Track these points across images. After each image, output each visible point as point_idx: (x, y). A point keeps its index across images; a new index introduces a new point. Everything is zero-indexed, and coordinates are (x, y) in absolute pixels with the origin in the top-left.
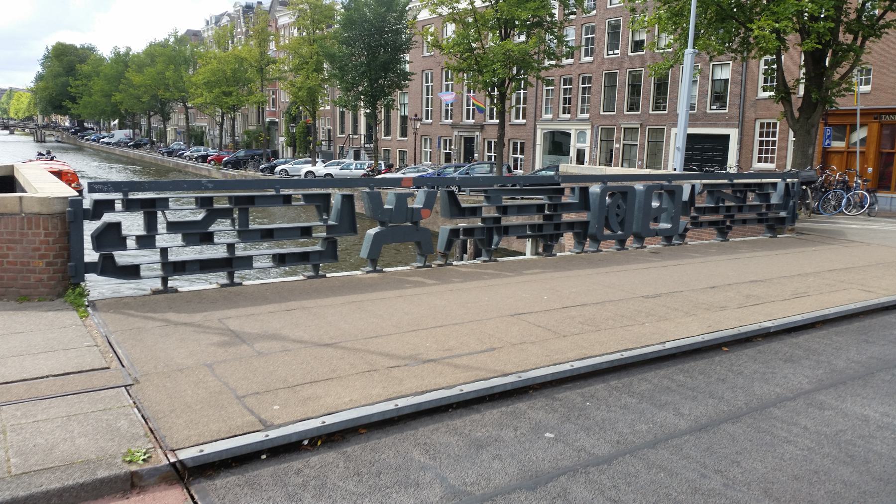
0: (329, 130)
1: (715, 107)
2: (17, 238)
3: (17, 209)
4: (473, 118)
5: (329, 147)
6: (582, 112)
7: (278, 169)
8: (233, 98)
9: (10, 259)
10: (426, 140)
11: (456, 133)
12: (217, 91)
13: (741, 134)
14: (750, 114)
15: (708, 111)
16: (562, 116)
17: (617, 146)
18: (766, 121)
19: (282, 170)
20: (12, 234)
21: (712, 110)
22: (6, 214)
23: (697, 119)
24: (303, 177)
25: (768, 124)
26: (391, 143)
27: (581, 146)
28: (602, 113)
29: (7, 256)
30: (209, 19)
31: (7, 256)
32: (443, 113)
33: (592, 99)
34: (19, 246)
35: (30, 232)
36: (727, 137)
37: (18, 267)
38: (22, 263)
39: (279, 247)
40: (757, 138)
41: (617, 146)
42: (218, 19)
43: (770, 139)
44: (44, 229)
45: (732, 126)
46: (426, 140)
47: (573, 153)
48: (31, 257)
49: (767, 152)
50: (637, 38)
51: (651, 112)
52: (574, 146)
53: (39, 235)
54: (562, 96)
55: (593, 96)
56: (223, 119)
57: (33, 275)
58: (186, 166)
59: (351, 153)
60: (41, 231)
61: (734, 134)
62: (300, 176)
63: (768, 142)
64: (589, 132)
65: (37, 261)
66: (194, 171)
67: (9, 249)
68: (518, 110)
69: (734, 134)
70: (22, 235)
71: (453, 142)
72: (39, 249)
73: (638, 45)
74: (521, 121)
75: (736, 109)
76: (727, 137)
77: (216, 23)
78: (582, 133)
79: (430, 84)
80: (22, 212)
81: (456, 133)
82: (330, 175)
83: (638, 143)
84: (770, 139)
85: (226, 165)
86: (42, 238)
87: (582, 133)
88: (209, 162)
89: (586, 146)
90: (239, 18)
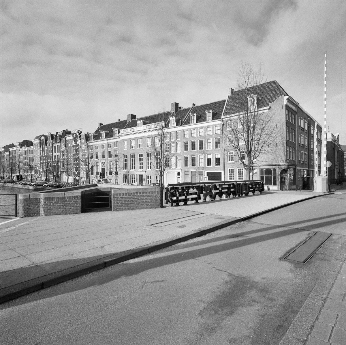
16: (229, 162)
32: (131, 168)
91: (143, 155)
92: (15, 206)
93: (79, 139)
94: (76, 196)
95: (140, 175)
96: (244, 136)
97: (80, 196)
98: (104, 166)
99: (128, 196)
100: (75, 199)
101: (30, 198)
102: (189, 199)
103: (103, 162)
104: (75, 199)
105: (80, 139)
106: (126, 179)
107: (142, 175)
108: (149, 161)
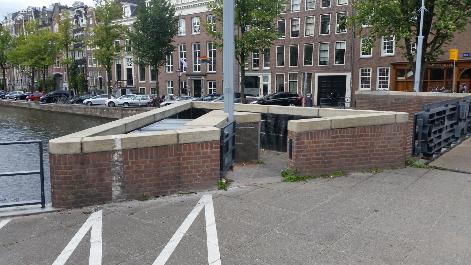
0: (100, 79)
1: (337, 63)
2: (392, 136)
3: (393, 122)
4: (199, 70)
5: (101, 87)
6: (265, 66)
7: (85, 101)
8: (46, 61)
9: (388, 148)
10: (169, 82)
11: (189, 78)
12: (36, 58)
13: (352, 75)
14: (357, 65)
15: (334, 65)
16: (254, 68)
17: (286, 83)
18: (382, 68)
19: (88, 102)
20: (390, 134)
21: (336, 64)
22: (389, 124)
23: (329, 69)
24: (107, 105)
25: (366, 70)
26: (146, 85)
27: (265, 83)
28: (276, 67)
29: (387, 146)
30: (6, 16)
31: (387, 146)
32: (208, 68)
33: (271, 60)
34: (392, 141)
35: (398, 133)
36: (345, 77)
37: (391, 151)
38: (393, 150)
39: (68, 145)
40: (360, 77)
41: (286, 83)
42: (15, 15)
43: (367, 77)
44: (404, 131)
45: (348, 72)
46: (169, 82)
47: (261, 87)
48: (397, 146)
49: (383, 82)
50: (294, 30)
51: (304, 66)
52: (261, 83)
53: (401, 133)
54: (253, 59)
55: (271, 58)
56: (33, 74)
57: (397, 155)
58: (10, 102)
59: (120, 91)
60: (403, 132)
61: (348, 75)
62: (104, 104)
63: (366, 78)
64: (270, 77)
65: (399, 147)
66: (16, 105)
67: (388, 142)
68: (169, 67)
69: (348, 75)
70: (394, 134)
71: (188, 83)
72: (400, 141)
73: (295, 34)
74: (171, 72)
75: (349, 64)
76: (345, 77)
77: (13, 18)
78: (266, 78)
79: (183, 52)
80: (395, 122)
81: (189, 78)
82: (127, 103)
83: (298, 81)
84: (367, 77)
85: (42, 100)
86: (402, 135)
87: (266, 78)
88: (27, 100)
89: (269, 83)
90: (31, 15)
91: (201, 47)
92: (38, 177)
93: (84, 17)
94: (207, 143)
95: (195, 81)
96: (33, 79)
97: (215, 142)
98: (131, 66)
99: (332, 137)
100: (205, 150)
101: (4, 71)
102: (432, 147)
103: (128, 59)
104: (205, 150)
105: (87, 18)
106: (212, 88)
107: (199, 82)
108: (213, 57)
